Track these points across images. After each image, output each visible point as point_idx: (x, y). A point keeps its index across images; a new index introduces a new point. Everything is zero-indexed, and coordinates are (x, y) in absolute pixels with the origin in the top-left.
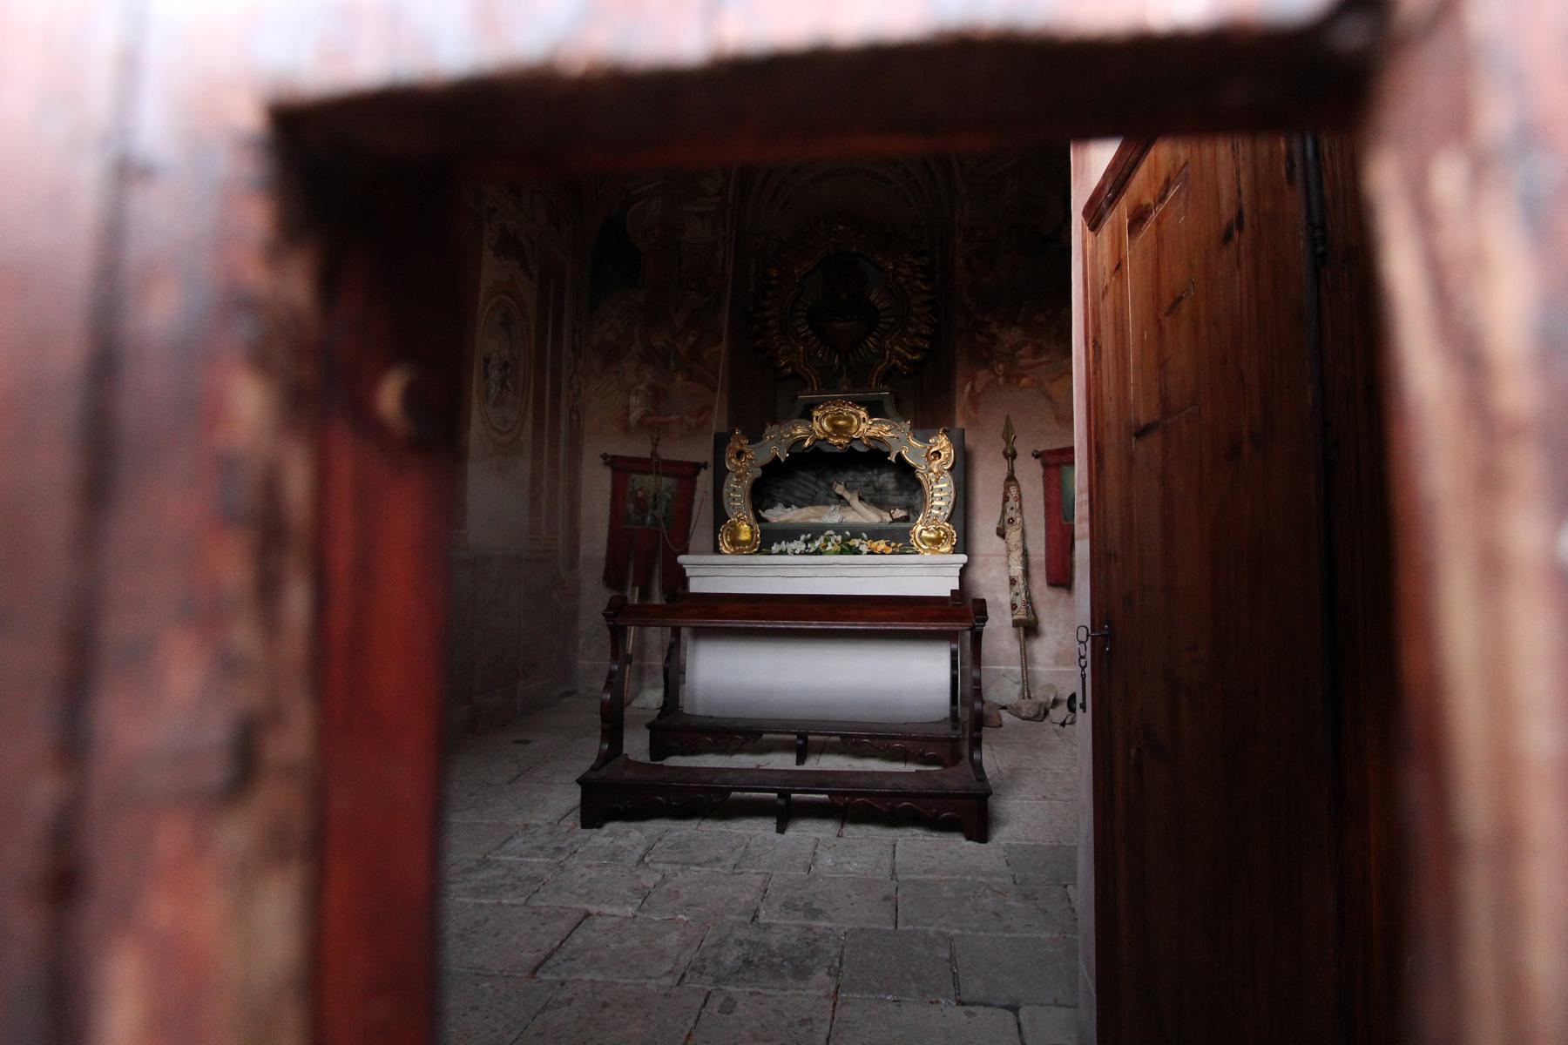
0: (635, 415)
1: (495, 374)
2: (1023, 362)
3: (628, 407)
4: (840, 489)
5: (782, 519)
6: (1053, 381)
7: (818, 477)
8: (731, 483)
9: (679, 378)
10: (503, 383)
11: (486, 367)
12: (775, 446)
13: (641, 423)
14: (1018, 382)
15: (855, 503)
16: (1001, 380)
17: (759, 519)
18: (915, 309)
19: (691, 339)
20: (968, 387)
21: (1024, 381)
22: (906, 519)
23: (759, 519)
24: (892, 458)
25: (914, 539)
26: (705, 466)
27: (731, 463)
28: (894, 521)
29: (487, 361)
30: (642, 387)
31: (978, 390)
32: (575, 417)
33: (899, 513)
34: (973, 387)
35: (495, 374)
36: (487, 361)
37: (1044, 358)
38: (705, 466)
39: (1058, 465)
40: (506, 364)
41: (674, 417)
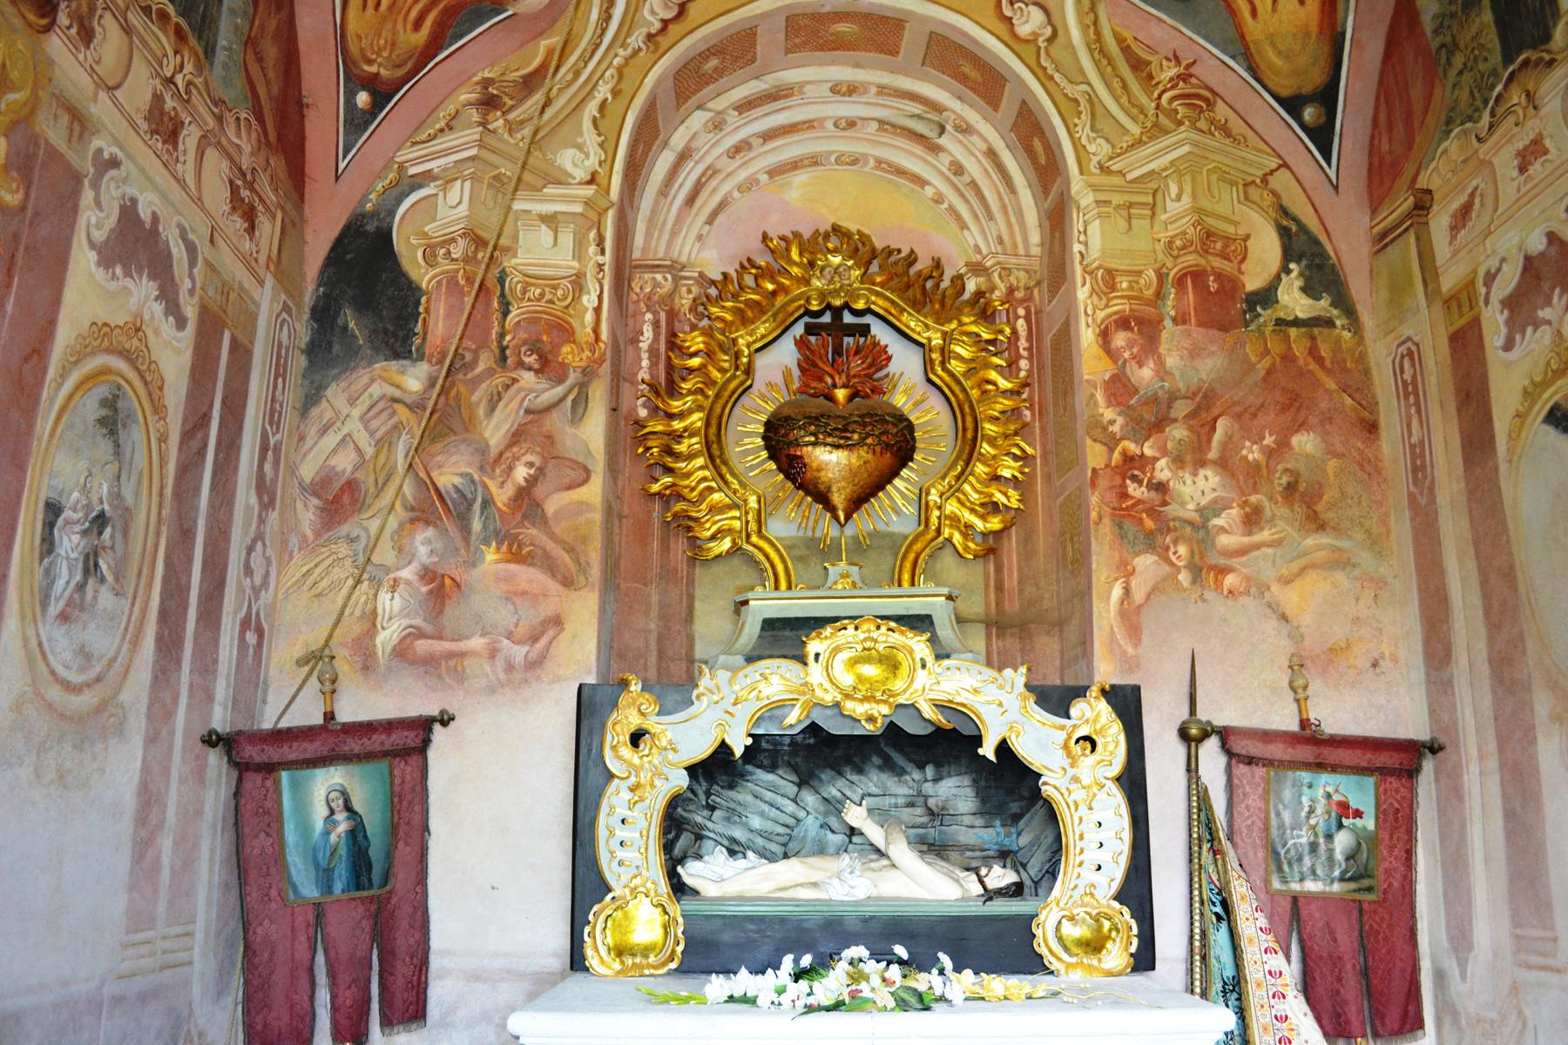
0: (387, 637)
1: (70, 543)
2: (1224, 541)
3: (374, 613)
4: (855, 815)
5: (731, 889)
6: (1287, 581)
7: (800, 785)
8: (616, 800)
9: (491, 555)
10: (90, 566)
11: (49, 525)
12: (736, 701)
13: (401, 652)
14: (1218, 586)
15: (901, 851)
16: (1184, 578)
17: (679, 888)
18: (986, 448)
19: (521, 473)
20: (1117, 592)
21: (1230, 580)
22: (1016, 890)
23: (679, 888)
24: (988, 750)
25: (1045, 939)
26: (979, 402)
27: (617, 755)
28: (990, 895)
29: (53, 510)
30: (407, 573)
31: (1138, 596)
32: (251, 638)
33: (1000, 877)
34: (1127, 591)
35: (70, 543)
36: (53, 510)
37: (1265, 535)
38: (979, 402)
39: (270, 768)
40: (101, 520)
41: (477, 643)
